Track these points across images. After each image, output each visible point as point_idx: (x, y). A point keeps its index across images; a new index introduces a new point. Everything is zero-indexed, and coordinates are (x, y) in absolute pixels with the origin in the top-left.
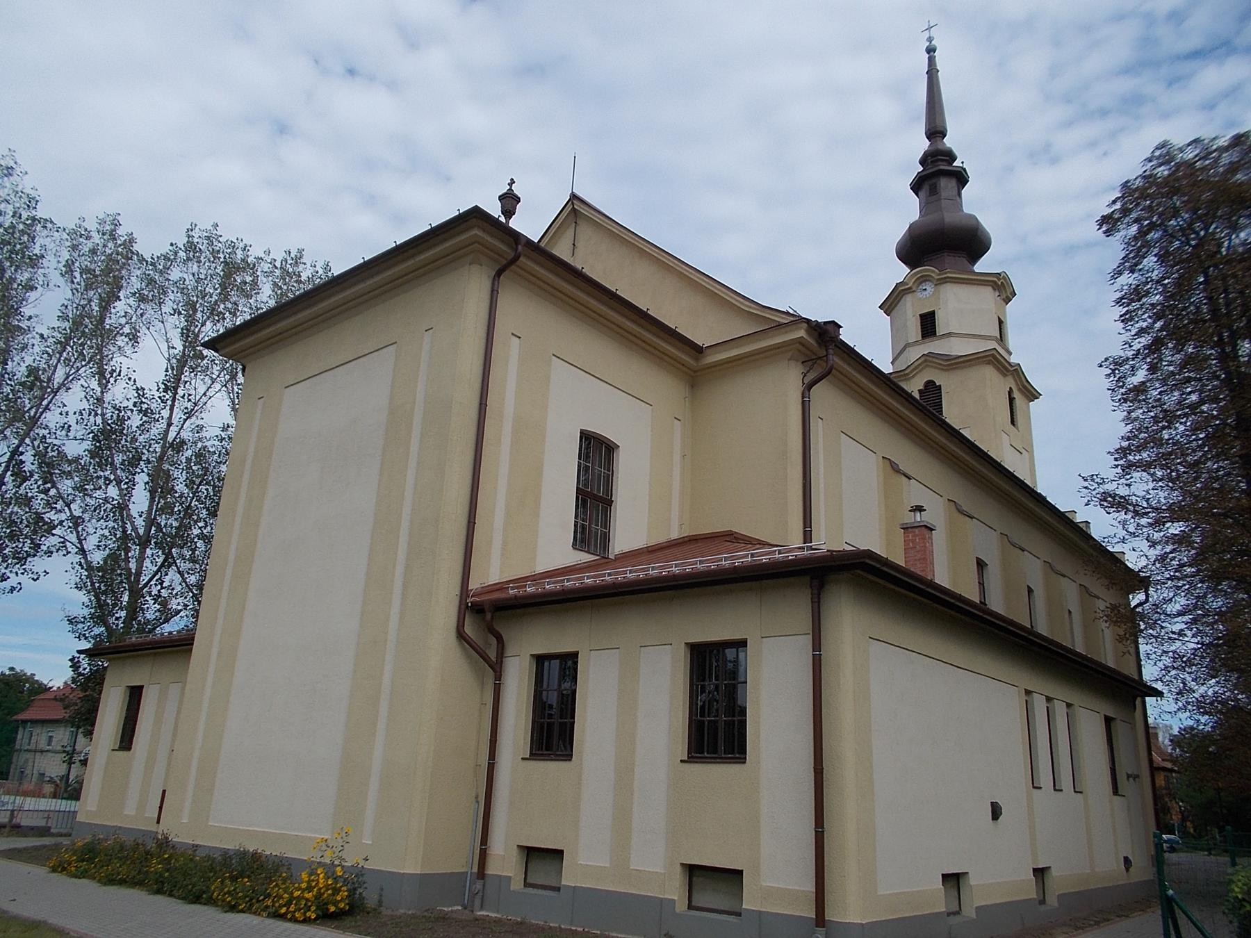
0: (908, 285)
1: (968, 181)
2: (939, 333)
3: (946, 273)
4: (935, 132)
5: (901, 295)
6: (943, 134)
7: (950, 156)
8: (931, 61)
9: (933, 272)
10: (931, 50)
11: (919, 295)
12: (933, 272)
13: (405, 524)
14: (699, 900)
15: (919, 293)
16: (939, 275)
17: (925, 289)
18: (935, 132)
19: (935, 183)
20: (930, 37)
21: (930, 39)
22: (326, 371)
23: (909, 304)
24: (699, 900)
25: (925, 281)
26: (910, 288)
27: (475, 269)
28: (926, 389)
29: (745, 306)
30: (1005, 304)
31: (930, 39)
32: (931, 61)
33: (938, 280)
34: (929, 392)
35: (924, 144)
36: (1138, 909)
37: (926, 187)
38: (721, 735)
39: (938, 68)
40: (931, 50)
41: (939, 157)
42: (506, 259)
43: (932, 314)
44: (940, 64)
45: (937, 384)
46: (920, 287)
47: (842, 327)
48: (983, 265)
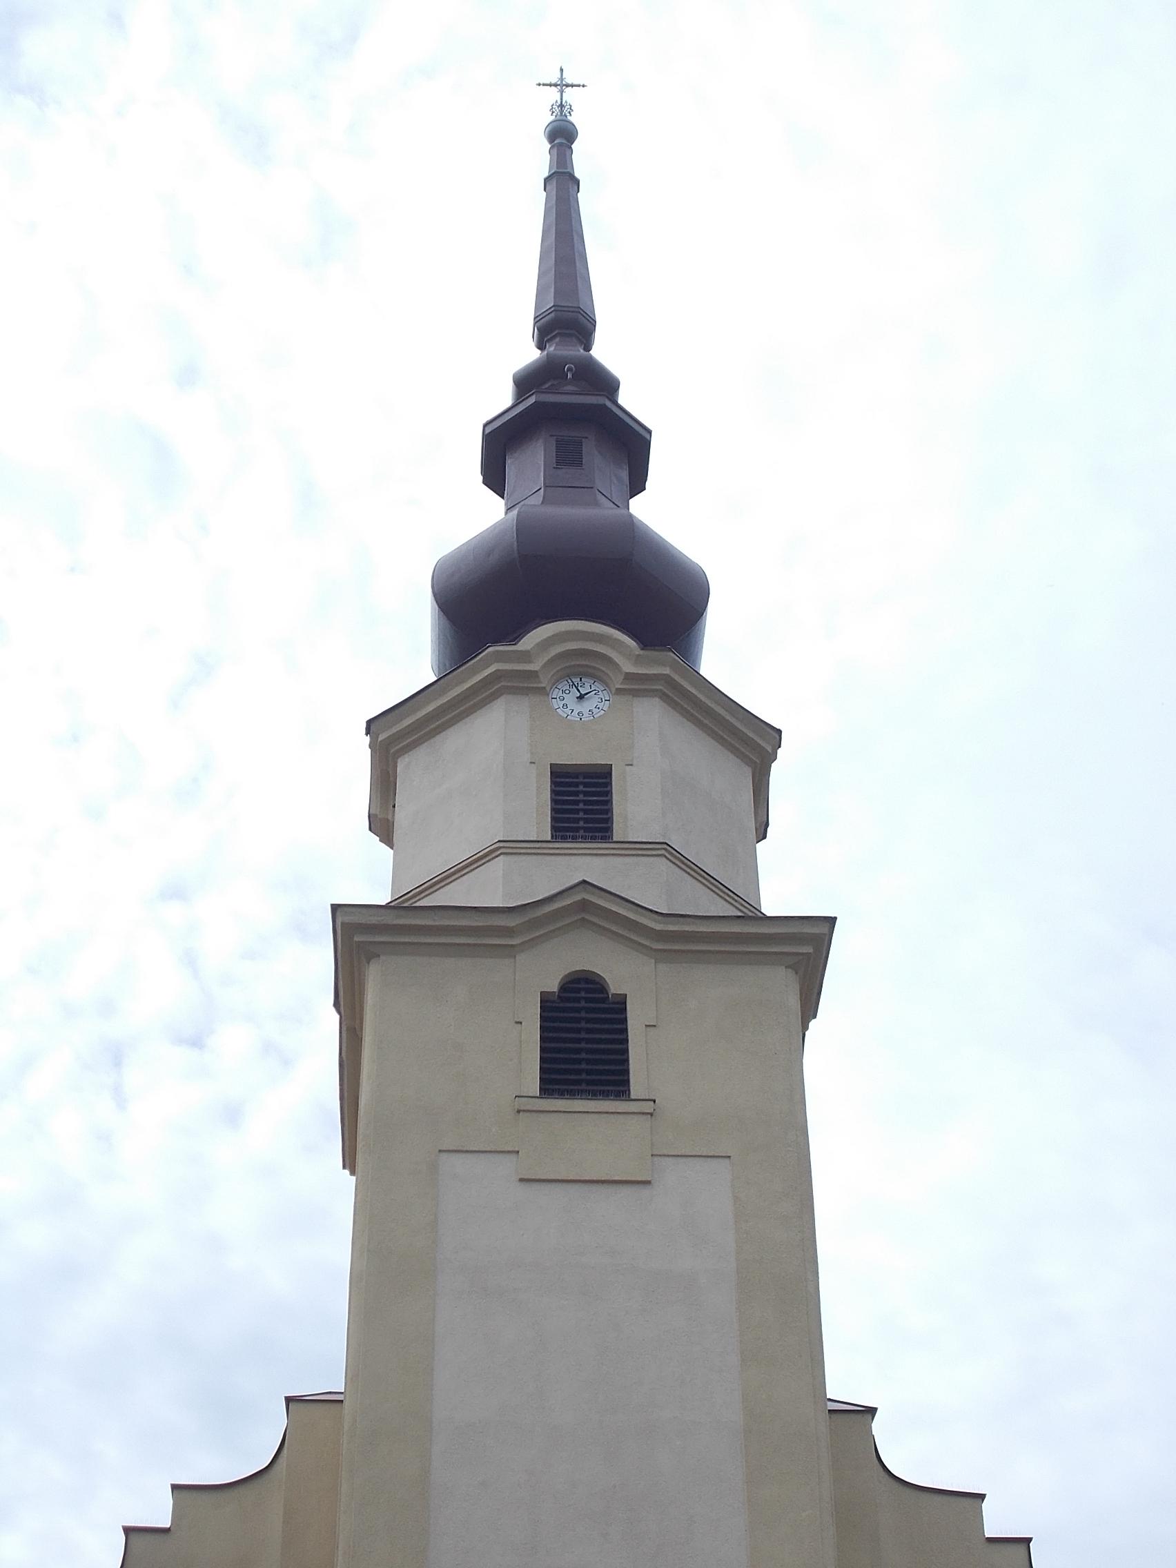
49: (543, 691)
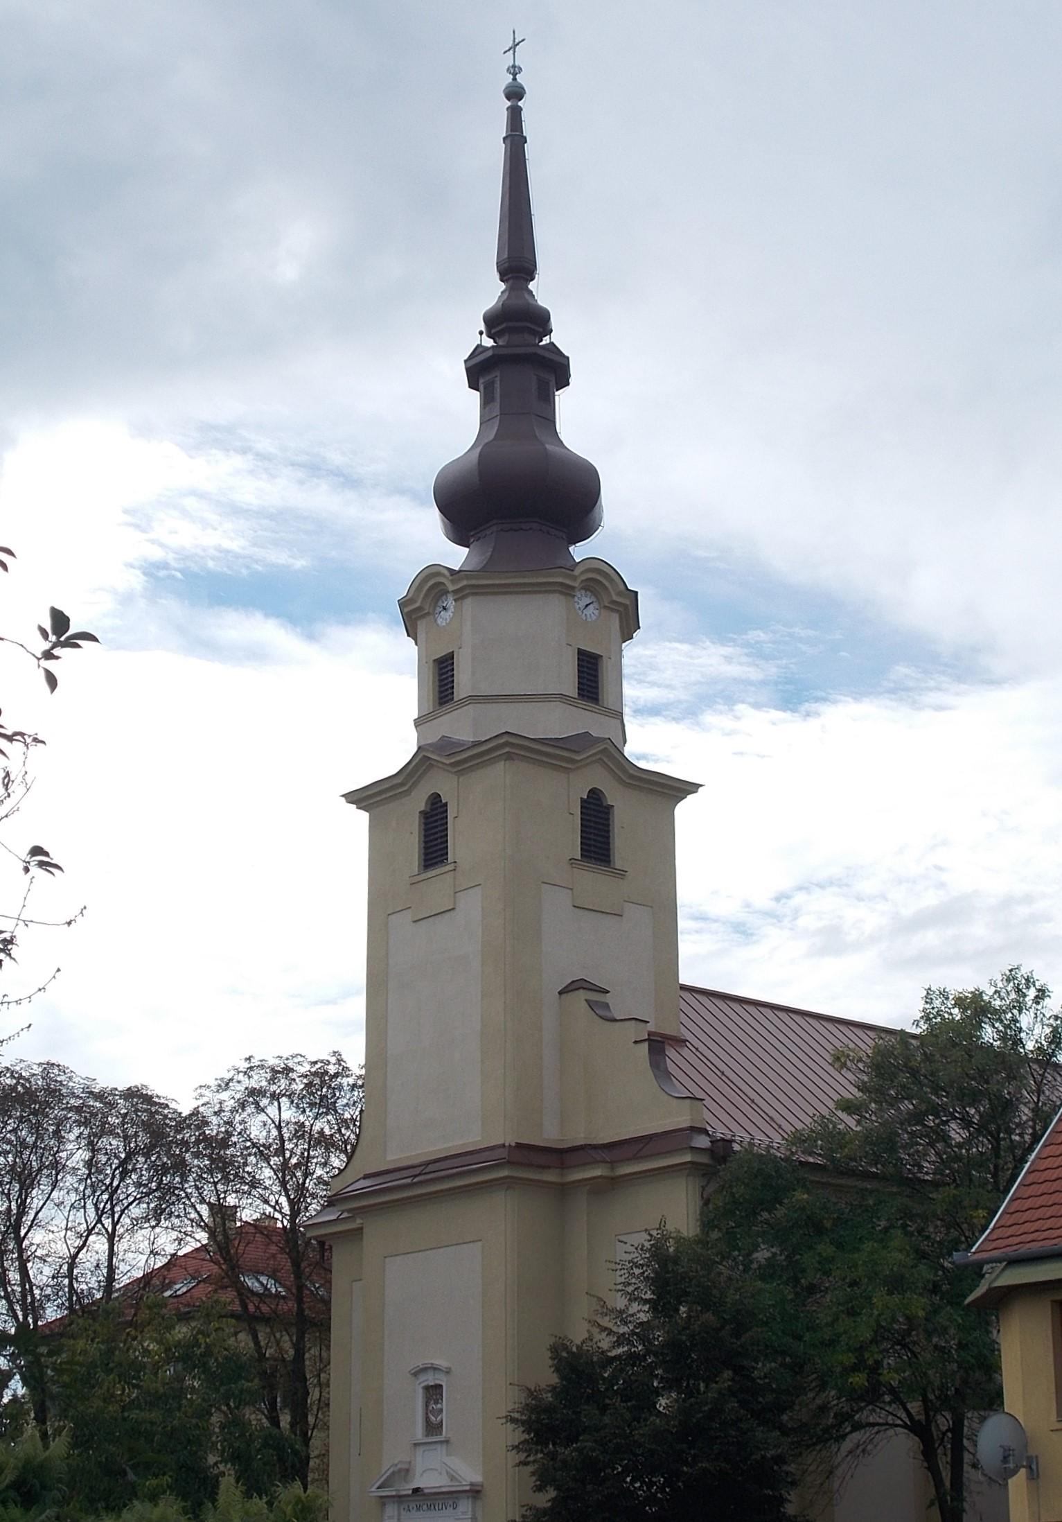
0: (415, 602)
2: (458, 695)
5: (468, 591)
7: (540, 321)
10: (515, 93)
20: (514, 66)
21: (515, 70)
22: (435, 915)
26: (419, 609)
28: (432, 810)
30: (620, 640)
31: (515, 70)
34: (436, 821)
35: (492, 291)
36: (324, 1354)
40: (515, 93)
42: (312, 1483)
43: (451, 656)
44: (529, 128)
45: (443, 801)
49: (428, 614)
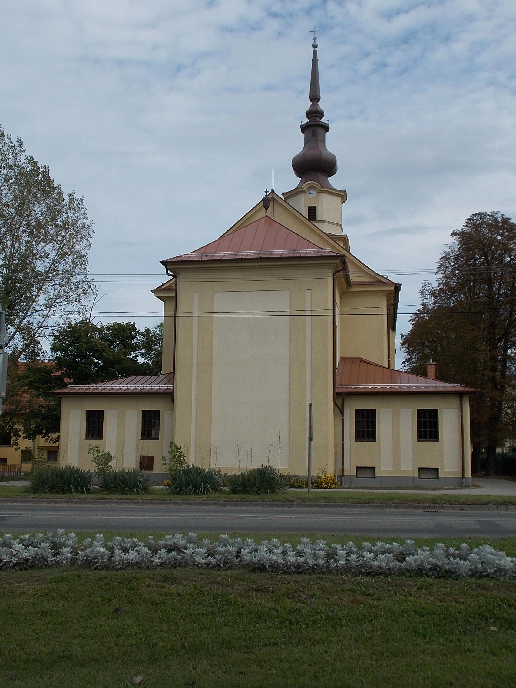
0: (303, 189)
1: (329, 131)
3: (324, 188)
4: (315, 98)
6: (318, 100)
8: (315, 53)
9: (318, 185)
10: (315, 46)
11: (308, 195)
12: (318, 185)
13: (308, 363)
14: (421, 476)
15: (308, 195)
16: (320, 188)
17: (312, 193)
18: (315, 98)
19: (315, 130)
20: (315, 37)
23: (303, 199)
24: (421, 476)
25: (312, 189)
26: (305, 191)
27: (330, 271)
29: (366, 270)
32: (315, 53)
33: (320, 190)
37: (309, 131)
38: (428, 434)
39: (318, 58)
41: (318, 115)
46: (309, 191)
47: (401, 284)
48: (332, 181)
